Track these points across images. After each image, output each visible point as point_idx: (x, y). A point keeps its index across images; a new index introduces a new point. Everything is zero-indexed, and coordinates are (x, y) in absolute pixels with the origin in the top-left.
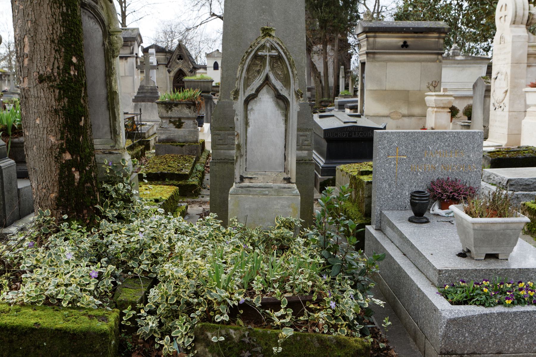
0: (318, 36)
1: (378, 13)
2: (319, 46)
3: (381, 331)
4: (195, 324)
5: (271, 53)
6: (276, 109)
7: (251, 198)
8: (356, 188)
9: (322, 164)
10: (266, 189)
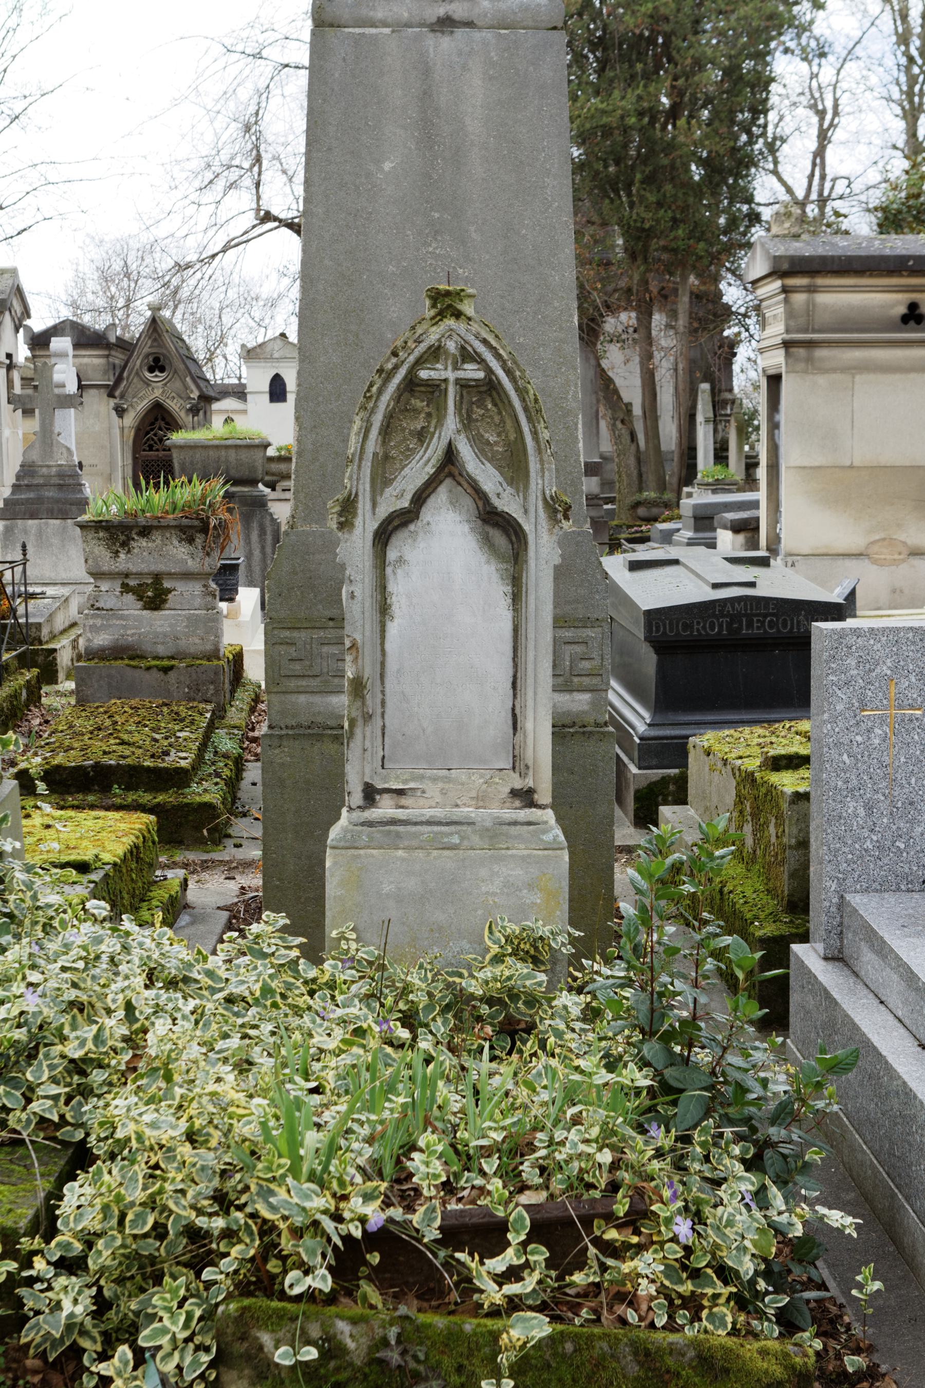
0: (622, 284)
1: (823, 201)
2: (623, 316)
3: (848, 1310)
4: (217, 1305)
5: (461, 374)
6: (483, 558)
7: (403, 860)
8: (755, 816)
9: (641, 728)
10: (452, 828)
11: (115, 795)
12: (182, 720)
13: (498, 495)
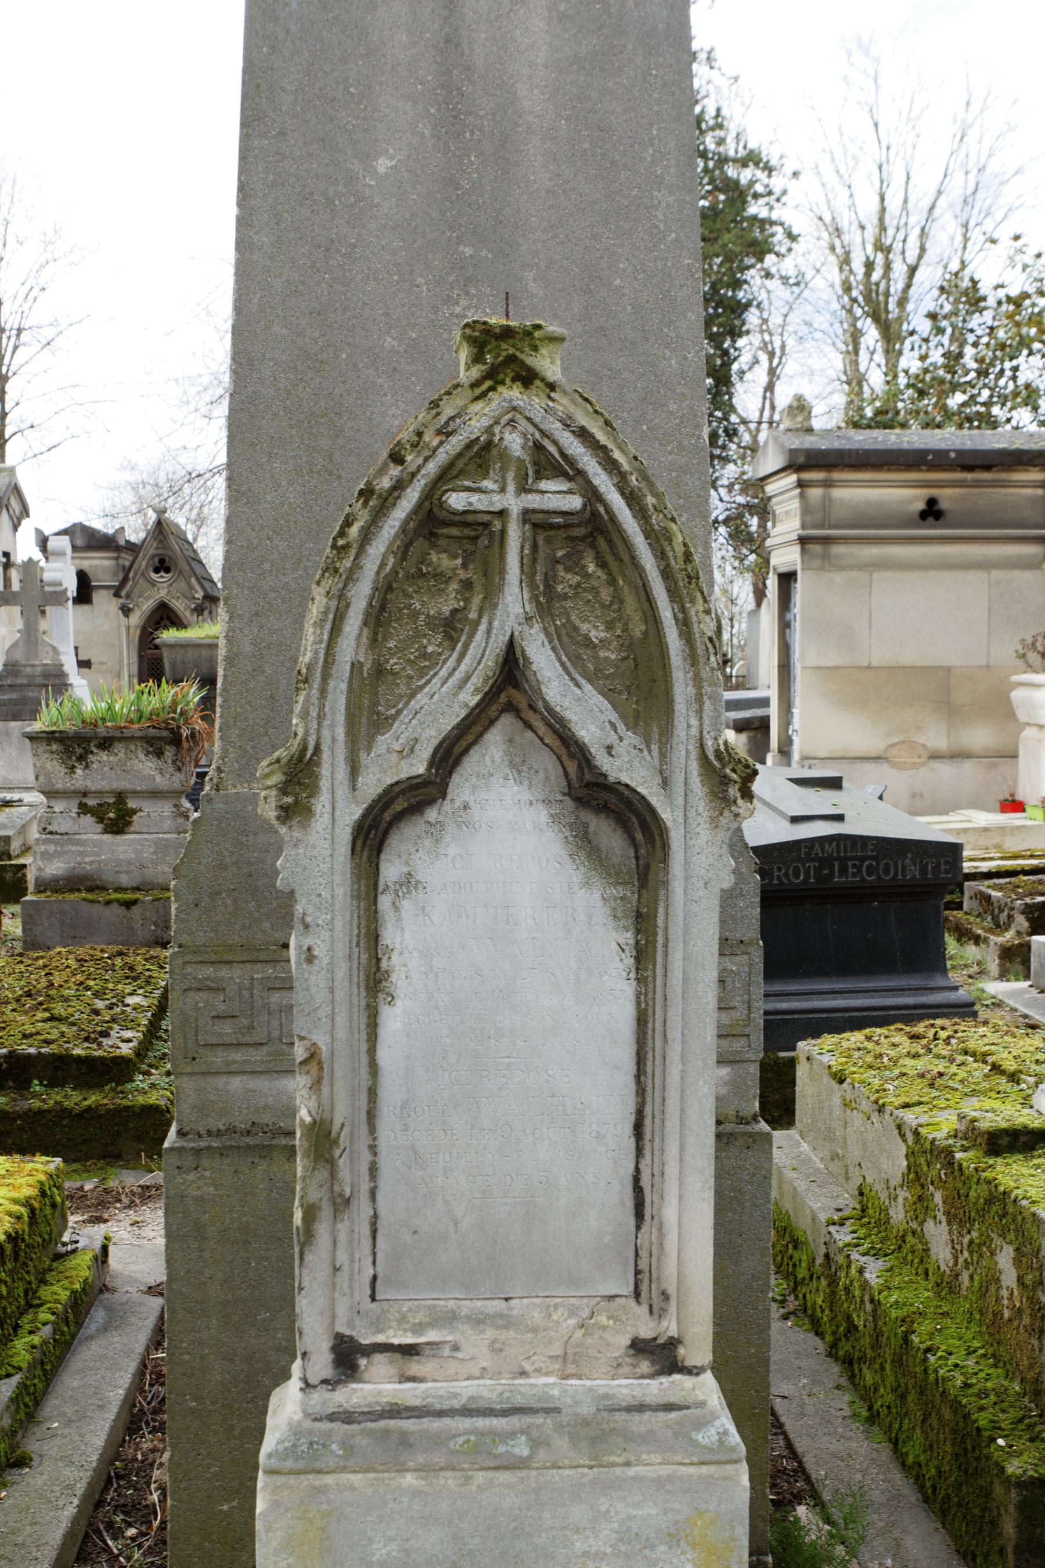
5: (533, 501)
6: (577, 877)
7: (415, 1493)
11: (35, 1095)
12: (135, 979)
13: (609, 749)
